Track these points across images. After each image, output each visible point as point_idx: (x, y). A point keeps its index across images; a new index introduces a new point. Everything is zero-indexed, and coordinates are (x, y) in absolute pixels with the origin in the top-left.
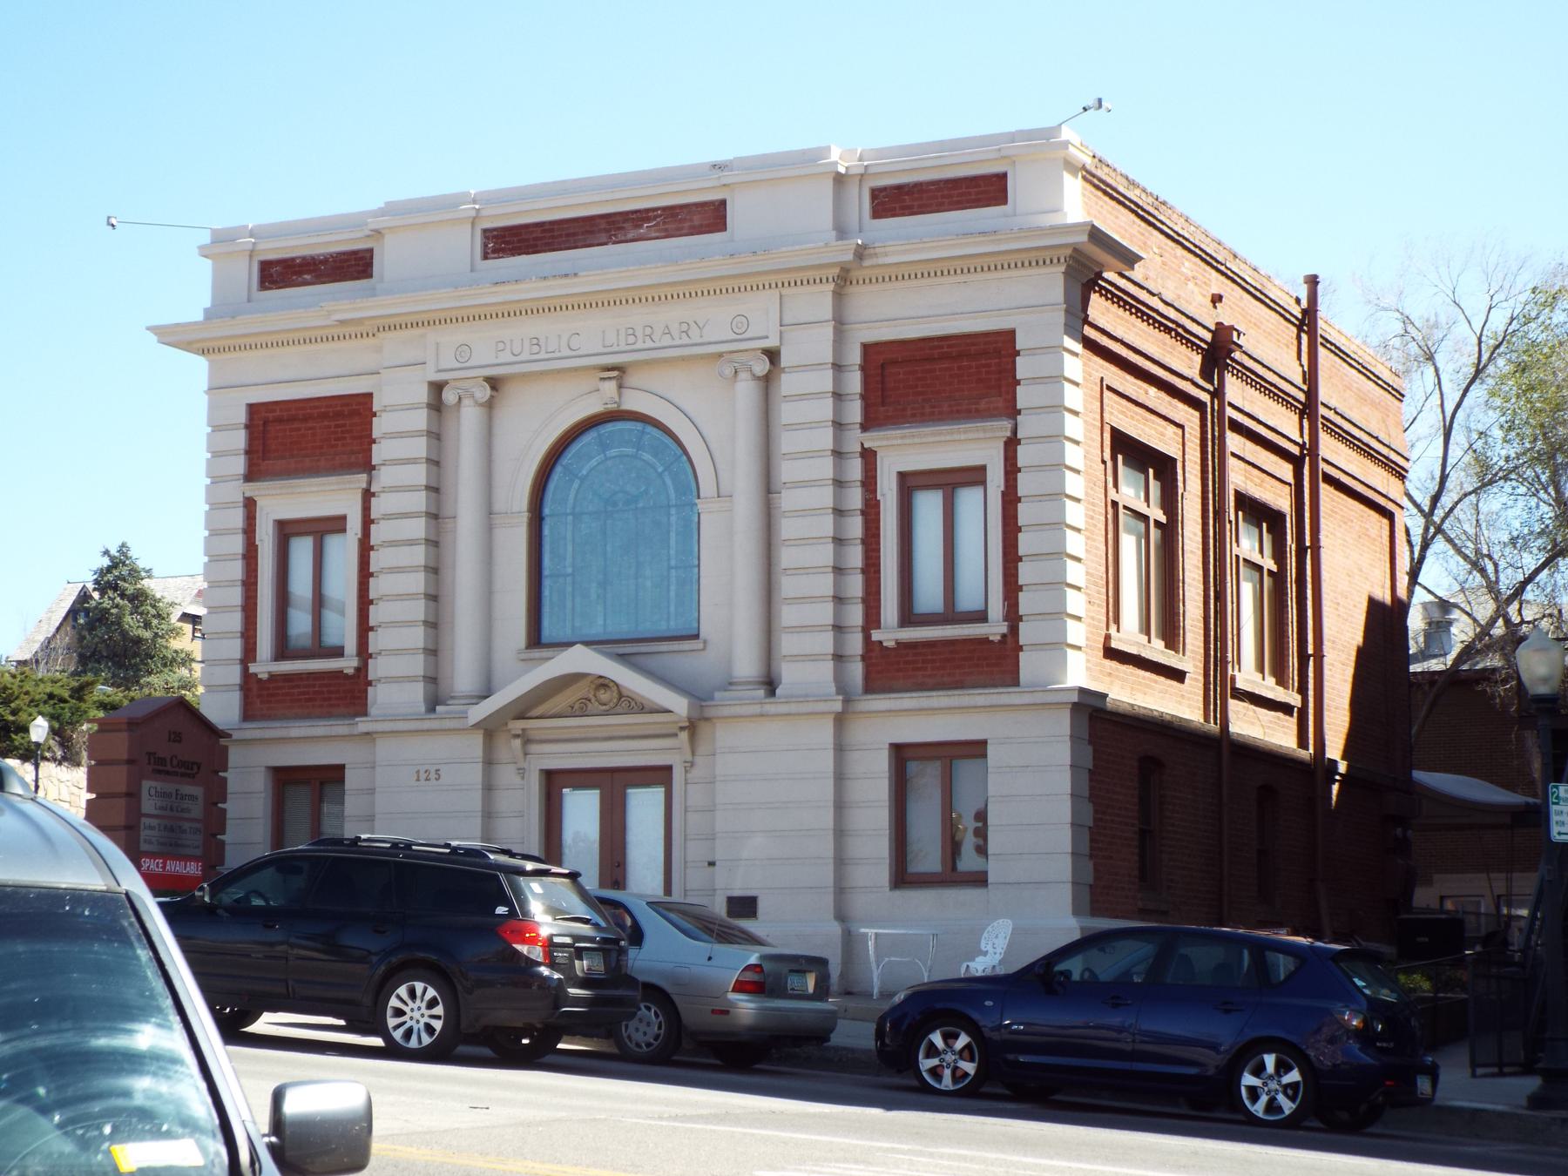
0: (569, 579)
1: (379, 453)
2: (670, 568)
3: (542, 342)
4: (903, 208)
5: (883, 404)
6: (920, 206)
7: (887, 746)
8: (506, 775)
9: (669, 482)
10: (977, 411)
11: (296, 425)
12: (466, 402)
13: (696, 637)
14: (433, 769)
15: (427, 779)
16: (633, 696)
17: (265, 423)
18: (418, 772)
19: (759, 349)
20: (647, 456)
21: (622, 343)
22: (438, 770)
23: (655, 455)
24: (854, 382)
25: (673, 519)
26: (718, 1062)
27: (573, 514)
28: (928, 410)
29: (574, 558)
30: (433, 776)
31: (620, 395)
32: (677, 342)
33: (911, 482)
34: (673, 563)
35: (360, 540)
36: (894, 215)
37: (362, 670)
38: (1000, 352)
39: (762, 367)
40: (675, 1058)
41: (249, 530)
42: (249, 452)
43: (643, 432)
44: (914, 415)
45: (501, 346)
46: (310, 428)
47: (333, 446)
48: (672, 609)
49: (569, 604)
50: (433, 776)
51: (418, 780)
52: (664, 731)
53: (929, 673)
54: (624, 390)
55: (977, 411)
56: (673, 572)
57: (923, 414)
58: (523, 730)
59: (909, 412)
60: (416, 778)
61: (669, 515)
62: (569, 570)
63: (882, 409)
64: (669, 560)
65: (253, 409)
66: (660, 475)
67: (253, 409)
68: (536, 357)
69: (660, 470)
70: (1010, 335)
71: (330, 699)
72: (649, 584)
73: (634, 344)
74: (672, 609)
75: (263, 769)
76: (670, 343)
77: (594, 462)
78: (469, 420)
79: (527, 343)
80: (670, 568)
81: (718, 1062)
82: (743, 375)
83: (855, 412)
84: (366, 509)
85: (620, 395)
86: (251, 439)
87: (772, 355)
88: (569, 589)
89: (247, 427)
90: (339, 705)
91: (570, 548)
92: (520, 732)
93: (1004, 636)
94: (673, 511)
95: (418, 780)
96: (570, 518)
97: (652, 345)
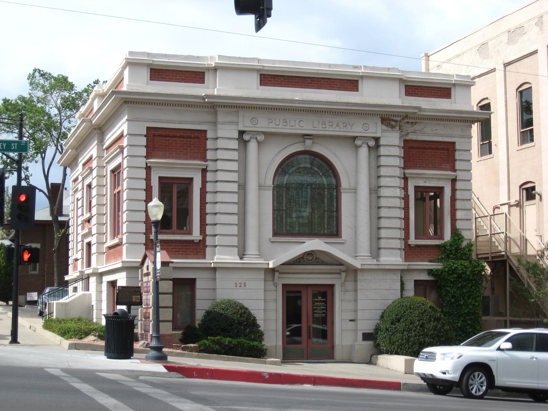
1: (210, 155)
3: (288, 122)
10: (441, 168)
15: (240, 286)
16: (299, 258)
18: (236, 283)
20: (315, 169)
22: (245, 283)
23: (319, 169)
25: (326, 193)
26: (532, 400)
27: (286, 187)
28: (424, 165)
29: (286, 204)
30: (243, 285)
38: (448, 149)
39: (372, 143)
40: (485, 397)
41: (148, 179)
43: (314, 160)
44: (420, 167)
46: (175, 141)
47: (186, 149)
48: (326, 226)
49: (284, 221)
51: (236, 286)
52: (325, 271)
53: (425, 256)
55: (441, 168)
60: (235, 286)
61: (324, 192)
68: (316, 129)
69: (321, 174)
70: (454, 143)
71: (186, 252)
72: (316, 216)
73: (278, 125)
74: (326, 226)
76: (339, 129)
77: (294, 169)
80: (325, 211)
81: (532, 400)
87: (377, 139)
88: (284, 215)
90: (190, 254)
91: (284, 200)
93: (200, 240)
94: (326, 190)
95: (236, 286)
96: (285, 189)
97: (347, 130)
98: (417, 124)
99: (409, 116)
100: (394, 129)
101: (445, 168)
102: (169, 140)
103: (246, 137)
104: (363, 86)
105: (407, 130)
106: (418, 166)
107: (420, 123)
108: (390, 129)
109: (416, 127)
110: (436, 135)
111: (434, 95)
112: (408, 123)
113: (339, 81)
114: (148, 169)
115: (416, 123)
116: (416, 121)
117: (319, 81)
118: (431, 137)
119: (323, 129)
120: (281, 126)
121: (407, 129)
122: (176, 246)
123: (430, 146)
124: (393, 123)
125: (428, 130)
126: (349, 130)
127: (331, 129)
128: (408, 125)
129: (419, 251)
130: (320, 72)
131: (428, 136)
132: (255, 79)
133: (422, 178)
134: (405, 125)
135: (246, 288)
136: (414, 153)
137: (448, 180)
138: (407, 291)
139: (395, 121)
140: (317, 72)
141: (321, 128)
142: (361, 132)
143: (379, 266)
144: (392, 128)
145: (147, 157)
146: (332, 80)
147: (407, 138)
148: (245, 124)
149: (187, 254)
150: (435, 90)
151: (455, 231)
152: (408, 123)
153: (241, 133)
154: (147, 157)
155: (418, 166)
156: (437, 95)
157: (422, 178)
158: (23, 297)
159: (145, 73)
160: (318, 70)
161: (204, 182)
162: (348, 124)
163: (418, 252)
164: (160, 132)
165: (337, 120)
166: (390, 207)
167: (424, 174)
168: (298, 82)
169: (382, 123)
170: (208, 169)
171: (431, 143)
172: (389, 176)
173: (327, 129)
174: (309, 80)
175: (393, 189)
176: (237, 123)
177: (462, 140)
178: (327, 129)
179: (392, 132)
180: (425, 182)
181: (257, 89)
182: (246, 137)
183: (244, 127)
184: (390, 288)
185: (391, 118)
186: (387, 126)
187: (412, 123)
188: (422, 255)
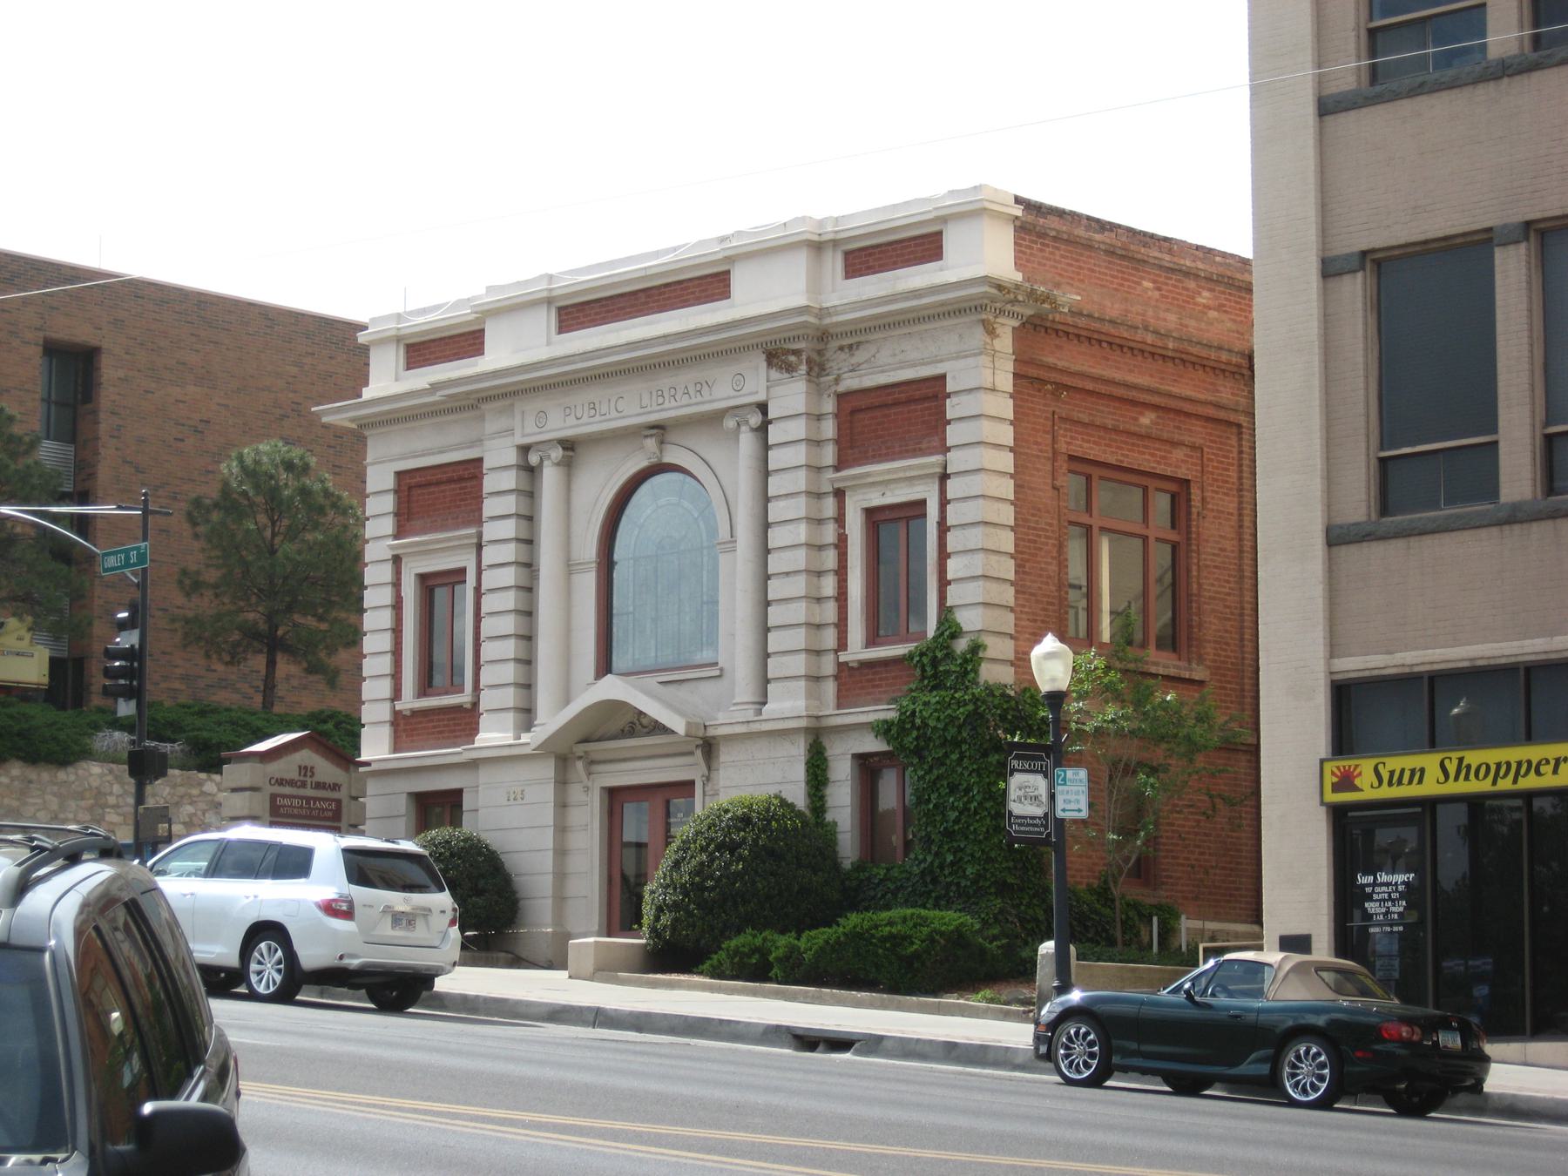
0: (631, 616)
1: (953, 434)
2: (703, 603)
3: (597, 407)
4: (869, 268)
5: (852, 448)
6: (880, 266)
7: (850, 756)
8: (576, 793)
9: (701, 524)
10: (920, 449)
11: (432, 489)
12: (546, 463)
13: (716, 664)
14: (519, 790)
17: (410, 488)
18: (509, 793)
19: (1325, 296)
20: (686, 504)
21: (654, 404)
24: (829, 429)
25: (705, 559)
30: (519, 797)
31: (661, 451)
32: (694, 400)
33: (431, 583)
34: (705, 598)
35: (938, 522)
36: (861, 275)
37: (476, 704)
42: (397, 514)
44: (874, 456)
45: (568, 411)
50: (519, 797)
54: (664, 446)
55: (920, 449)
56: (705, 607)
57: (880, 455)
58: (586, 752)
59: (871, 453)
62: (631, 609)
63: (850, 451)
64: (702, 596)
65: (400, 475)
66: (696, 519)
67: (400, 475)
70: (942, 378)
72: (688, 619)
75: (405, 795)
78: (550, 477)
79: (586, 408)
82: (743, 428)
83: (829, 455)
84: (943, 491)
85: (661, 451)
86: (399, 503)
87: (763, 408)
89: (396, 491)
92: (582, 754)
94: (705, 552)
98: (861, 347)
99: (831, 331)
100: (794, 374)
101: (929, 448)
102: (434, 493)
103: (533, 459)
104: (740, 281)
105: (839, 369)
106: (897, 449)
107: (867, 342)
108: (787, 375)
109: (860, 356)
110: (903, 365)
111: (923, 257)
112: (841, 348)
113: (697, 282)
114: (397, 560)
115: (859, 344)
116: (856, 339)
117: (660, 294)
118: (892, 373)
119: (659, 407)
120: (585, 419)
121: (840, 365)
122: (439, 720)
123: (896, 396)
124: (792, 358)
125: (884, 357)
126: (707, 397)
127: (673, 404)
128: (843, 356)
129: (870, 677)
130: (649, 272)
131: (883, 372)
132: (544, 320)
133: (873, 484)
134: (835, 356)
135: (524, 802)
136: (867, 422)
137: (930, 480)
138: (839, 783)
139: (796, 352)
140: (642, 274)
141: (655, 408)
142: (729, 398)
143: (751, 724)
144: (788, 371)
145: (398, 535)
146: (685, 285)
147: (841, 388)
148: (528, 431)
149: (456, 737)
150: (923, 244)
151: (945, 611)
152: (841, 348)
153: (525, 450)
154: (398, 535)
155: (897, 449)
156: (915, 259)
157: (873, 484)
158: (1039, 783)
159: (834, 263)
160: (645, 268)
161: (944, 503)
162: (704, 384)
163: (868, 681)
164: (418, 479)
165: (686, 378)
166: (787, 574)
167: (868, 475)
168: (623, 308)
169: (770, 364)
170: (948, 472)
171: (897, 390)
172: (787, 495)
173: (667, 405)
174: (642, 295)
175: (790, 527)
176: (510, 432)
177: (961, 363)
178: (667, 405)
179: (789, 383)
180: (883, 494)
181: (397, 380)
182: (533, 459)
183: (524, 436)
184: (784, 781)
185: (785, 346)
186: (781, 368)
187: (850, 347)
188: (877, 686)
